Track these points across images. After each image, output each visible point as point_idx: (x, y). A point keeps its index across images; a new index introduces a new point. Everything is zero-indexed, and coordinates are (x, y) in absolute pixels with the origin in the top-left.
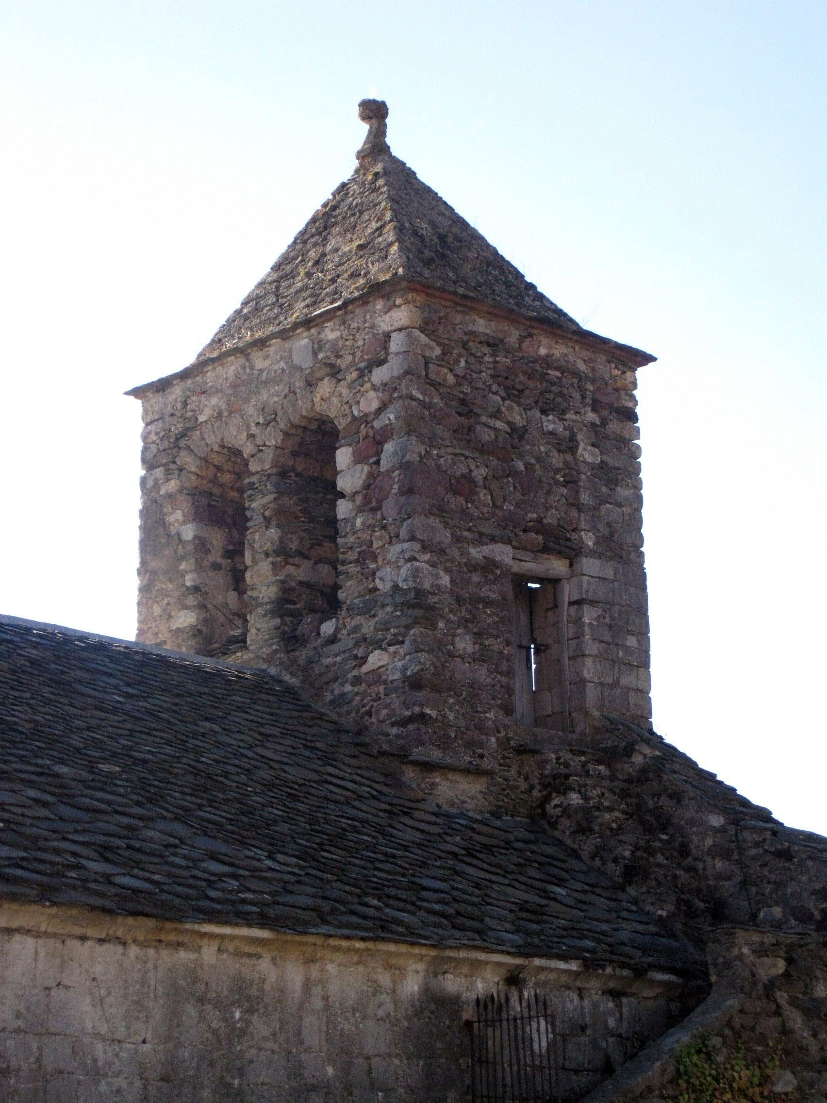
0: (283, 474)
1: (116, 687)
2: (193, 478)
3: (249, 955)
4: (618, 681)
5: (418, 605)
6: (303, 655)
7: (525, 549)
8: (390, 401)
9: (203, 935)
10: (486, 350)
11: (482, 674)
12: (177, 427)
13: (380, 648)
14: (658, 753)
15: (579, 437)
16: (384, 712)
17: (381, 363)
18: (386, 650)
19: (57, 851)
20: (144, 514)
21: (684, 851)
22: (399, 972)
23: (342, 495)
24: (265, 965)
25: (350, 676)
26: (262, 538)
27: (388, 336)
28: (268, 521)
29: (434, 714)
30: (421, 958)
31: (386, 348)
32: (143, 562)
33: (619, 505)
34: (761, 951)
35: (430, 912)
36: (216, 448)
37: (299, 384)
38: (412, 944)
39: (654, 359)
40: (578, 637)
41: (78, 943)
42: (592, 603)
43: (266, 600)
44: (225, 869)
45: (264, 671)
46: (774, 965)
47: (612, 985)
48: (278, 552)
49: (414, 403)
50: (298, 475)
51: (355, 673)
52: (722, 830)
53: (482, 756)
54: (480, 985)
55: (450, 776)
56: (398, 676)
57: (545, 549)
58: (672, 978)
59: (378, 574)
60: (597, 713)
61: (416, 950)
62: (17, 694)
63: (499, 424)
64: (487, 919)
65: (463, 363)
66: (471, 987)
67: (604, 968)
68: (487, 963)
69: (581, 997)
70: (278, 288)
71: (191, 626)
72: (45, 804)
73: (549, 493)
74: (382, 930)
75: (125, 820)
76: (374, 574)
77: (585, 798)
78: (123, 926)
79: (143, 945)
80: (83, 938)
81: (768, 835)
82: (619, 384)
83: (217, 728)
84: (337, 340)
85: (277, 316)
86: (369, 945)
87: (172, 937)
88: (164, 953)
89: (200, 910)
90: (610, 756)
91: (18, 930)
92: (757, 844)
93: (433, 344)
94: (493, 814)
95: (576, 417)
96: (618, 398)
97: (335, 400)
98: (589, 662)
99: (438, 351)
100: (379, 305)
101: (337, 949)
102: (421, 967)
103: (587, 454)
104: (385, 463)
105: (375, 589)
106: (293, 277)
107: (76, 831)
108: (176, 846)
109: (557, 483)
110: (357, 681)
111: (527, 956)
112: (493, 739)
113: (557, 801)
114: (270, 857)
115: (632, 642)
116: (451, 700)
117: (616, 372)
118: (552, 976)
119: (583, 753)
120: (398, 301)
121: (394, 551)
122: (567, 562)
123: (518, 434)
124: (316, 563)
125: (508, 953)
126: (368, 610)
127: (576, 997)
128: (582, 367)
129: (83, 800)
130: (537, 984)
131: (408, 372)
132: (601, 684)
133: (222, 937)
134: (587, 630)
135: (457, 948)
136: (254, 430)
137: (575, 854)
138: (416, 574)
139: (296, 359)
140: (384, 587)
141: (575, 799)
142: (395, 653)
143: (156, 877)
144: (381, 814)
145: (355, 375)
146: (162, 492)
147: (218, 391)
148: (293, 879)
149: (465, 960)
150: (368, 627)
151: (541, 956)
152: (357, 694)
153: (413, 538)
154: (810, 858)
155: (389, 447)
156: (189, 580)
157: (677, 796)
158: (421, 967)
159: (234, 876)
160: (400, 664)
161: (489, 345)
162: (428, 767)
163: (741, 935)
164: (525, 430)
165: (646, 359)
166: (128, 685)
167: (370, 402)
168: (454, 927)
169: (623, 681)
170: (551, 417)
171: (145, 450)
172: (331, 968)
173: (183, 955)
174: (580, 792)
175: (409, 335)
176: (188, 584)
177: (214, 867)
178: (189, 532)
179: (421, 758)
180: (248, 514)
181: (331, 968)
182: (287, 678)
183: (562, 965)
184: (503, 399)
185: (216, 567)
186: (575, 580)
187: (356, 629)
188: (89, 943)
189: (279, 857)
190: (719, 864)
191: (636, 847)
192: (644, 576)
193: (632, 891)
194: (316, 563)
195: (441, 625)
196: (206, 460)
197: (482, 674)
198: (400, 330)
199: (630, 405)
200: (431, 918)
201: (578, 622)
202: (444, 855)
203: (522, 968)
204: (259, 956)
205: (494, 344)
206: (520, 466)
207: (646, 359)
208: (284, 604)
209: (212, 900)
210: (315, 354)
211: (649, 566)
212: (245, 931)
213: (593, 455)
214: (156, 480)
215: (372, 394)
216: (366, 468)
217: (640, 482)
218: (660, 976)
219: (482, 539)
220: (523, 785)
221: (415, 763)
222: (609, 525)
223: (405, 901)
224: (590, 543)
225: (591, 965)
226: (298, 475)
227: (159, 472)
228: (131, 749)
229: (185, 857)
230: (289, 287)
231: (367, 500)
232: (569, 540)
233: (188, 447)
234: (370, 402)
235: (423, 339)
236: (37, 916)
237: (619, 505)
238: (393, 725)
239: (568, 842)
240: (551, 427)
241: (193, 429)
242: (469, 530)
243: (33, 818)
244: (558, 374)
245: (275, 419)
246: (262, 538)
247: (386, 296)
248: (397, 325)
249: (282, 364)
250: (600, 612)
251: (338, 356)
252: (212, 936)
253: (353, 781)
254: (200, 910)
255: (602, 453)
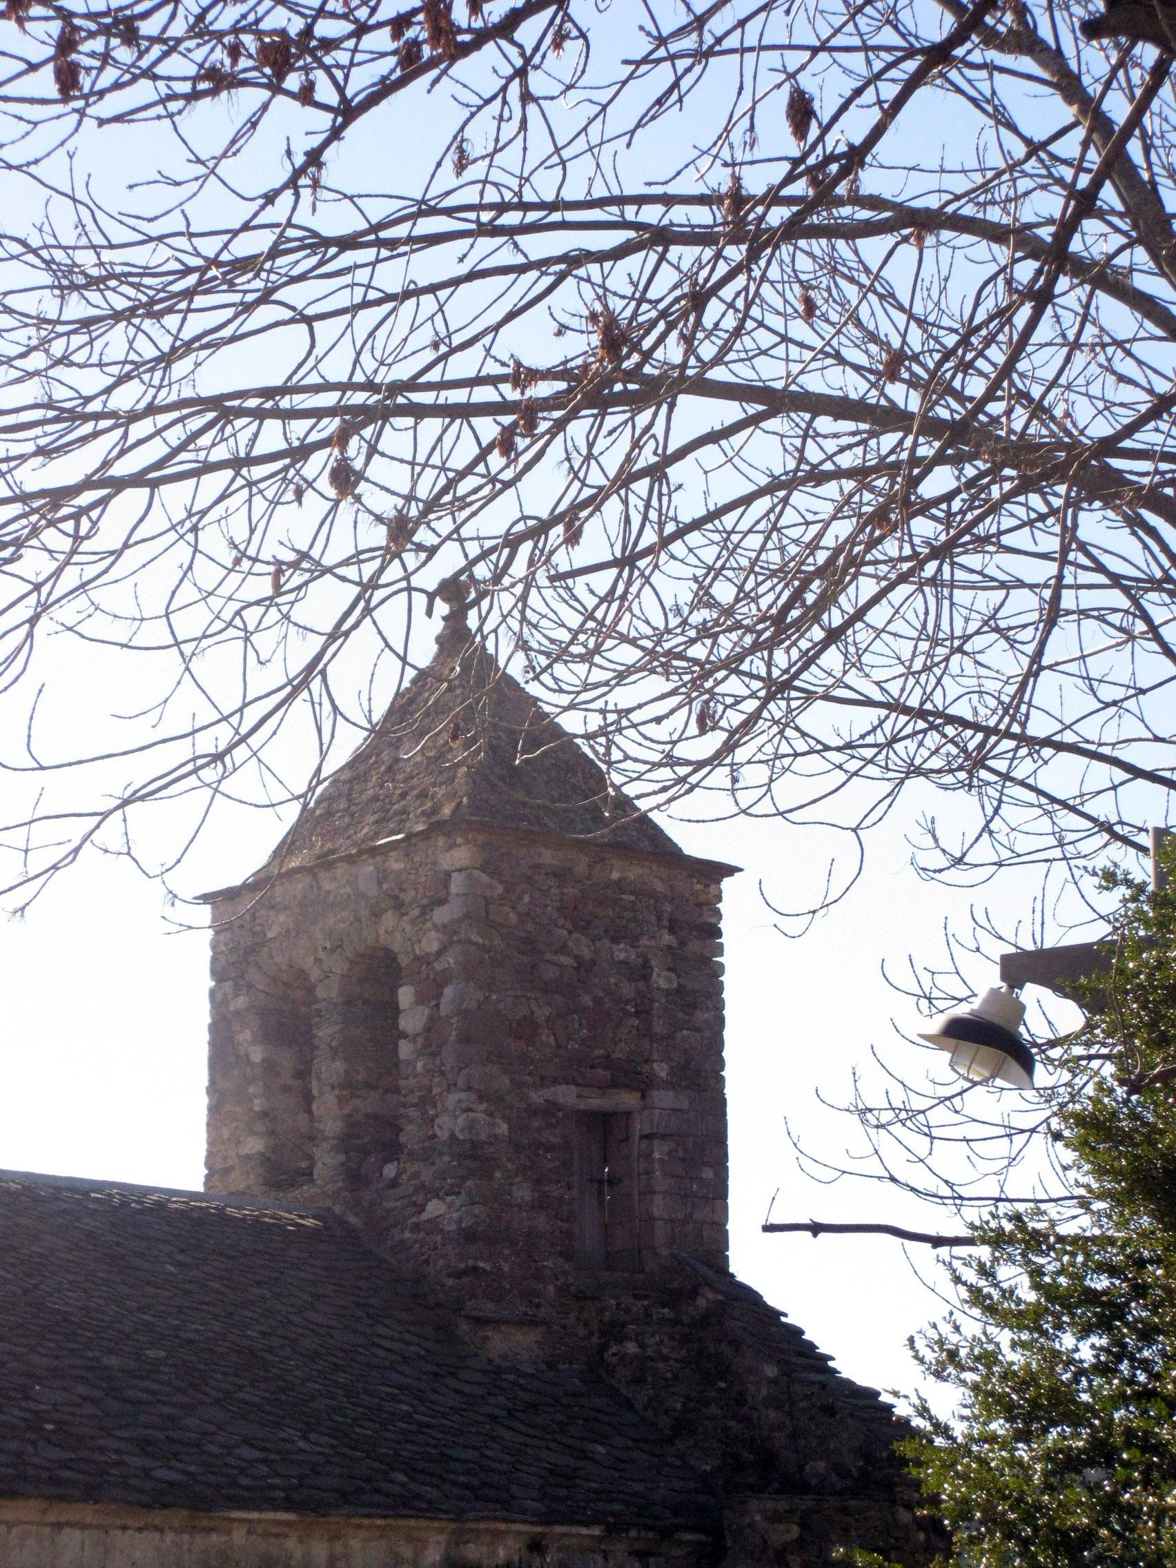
0: (350, 1002)
1: (169, 1255)
2: (262, 996)
3: (277, 1536)
4: (691, 1215)
5: (475, 1156)
6: (366, 1195)
7: (590, 1086)
8: (451, 944)
9: (234, 1520)
10: (552, 882)
11: (541, 1222)
12: (247, 941)
13: (437, 1196)
14: (720, 1297)
15: (653, 963)
16: (441, 1262)
17: (442, 902)
18: (443, 1199)
19: (102, 1450)
20: (214, 1028)
21: (741, 1399)
22: (422, 1544)
23: (404, 1035)
24: (291, 1544)
25: (410, 1222)
26: (329, 1069)
27: (448, 875)
28: (334, 1053)
29: (488, 1267)
30: (441, 1531)
31: (447, 887)
32: (212, 1081)
33: (698, 1030)
34: (775, 1518)
35: (454, 1483)
36: (284, 968)
37: (364, 913)
38: (432, 1519)
39: (741, 870)
40: (648, 1173)
41: (119, 1533)
42: (663, 1137)
43: (332, 1134)
44: (258, 1454)
45: (329, 1209)
46: (788, 1531)
47: (637, 1546)
48: (343, 1086)
49: (473, 948)
50: (366, 1002)
51: (414, 1220)
52: (774, 1382)
53: (538, 1306)
54: (502, 1552)
55: (503, 1328)
56: (453, 1227)
57: (614, 1085)
58: (702, 1537)
59: (437, 1121)
60: (665, 1252)
61: (437, 1524)
62: (70, 1277)
63: (565, 960)
64: (514, 1487)
65: (527, 899)
66: (494, 1553)
67: (627, 1531)
68: (508, 1532)
69: (605, 1558)
70: (351, 790)
71: (260, 1153)
72: (93, 1401)
73: (617, 1027)
74: (405, 1505)
75: (167, 1410)
76: (433, 1121)
77: (642, 1346)
78: (157, 1517)
79: (178, 1531)
80: (124, 1528)
81: (816, 1388)
82: (702, 898)
83: (268, 1294)
84: (400, 871)
85: (348, 827)
86: (390, 1521)
87: (205, 1523)
88: (198, 1537)
89: (230, 1498)
90: (674, 1298)
91: (68, 1524)
92: (807, 1397)
93: (495, 883)
94: (548, 1364)
95: (652, 943)
96: (701, 915)
97: (398, 935)
98: (658, 1199)
99: (500, 890)
100: (441, 841)
101: (359, 1527)
102: (442, 1538)
103: (662, 980)
104: (444, 1010)
105: (434, 1136)
106: (366, 781)
107: (120, 1427)
108: (214, 1434)
109: (627, 1013)
110: (416, 1228)
111: (548, 1524)
112: (551, 1288)
113: (614, 1349)
114: (304, 1437)
115: (708, 1173)
116: (506, 1252)
117: (699, 887)
118: (574, 1541)
119: (646, 1297)
120: (459, 840)
121: (453, 1098)
122: (639, 1095)
123: (585, 967)
124: (386, 1092)
125: (531, 1523)
126: (427, 1156)
127: (600, 1560)
128: (659, 886)
129: (130, 1392)
130: (559, 1549)
131: (467, 916)
132: (672, 1221)
133: (251, 1521)
134: (657, 1166)
135: (477, 1520)
136: (321, 955)
137: (630, 1405)
138: (471, 1125)
139: (362, 886)
140: (443, 1135)
141: (631, 1348)
142: (453, 1202)
143: (192, 1468)
144: (425, 1377)
145: (417, 912)
146: (232, 1008)
147: (287, 908)
148: (322, 1459)
149: (487, 1530)
150: (427, 1175)
151: (562, 1523)
152: (416, 1241)
153: (469, 1089)
154: (851, 1415)
155: (448, 992)
156: (258, 1105)
157: (735, 1344)
158: (442, 1538)
159: (265, 1461)
160: (455, 1215)
161: (555, 875)
162: (480, 1322)
163: (753, 1505)
164: (594, 962)
165: (731, 870)
166: (182, 1251)
167: (431, 943)
168: (477, 1498)
169: (697, 1215)
170: (622, 946)
171: (214, 960)
172: (355, 1544)
173: (214, 1538)
174: (637, 1341)
175: (469, 877)
176: (257, 1109)
177: (246, 1452)
178: (257, 1054)
179: (474, 1313)
180: (315, 1041)
181: (355, 1544)
182: (352, 1219)
183: (584, 1531)
184: (570, 933)
185: (286, 1089)
186: (645, 1113)
187: (415, 1175)
188: (130, 1532)
189: (312, 1436)
190: (772, 1414)
191: (689, 1399)
192: (723, 1102)
193: (680, 1445)
194: (386, 1092)
195: (498, 1175)
196: (274, 979)
197: (541, 1222)
198: (460, 870)
199: (713, 920)
200: (455, 1491)
201: (649, 1156)
202: (481, 1418)
203: (543, 1535)
204: (286, 1536)
205: (562, 875)
206: (587, 1000)
207: (731, 870)
208: (346, 1142)
209: (242, 1487)
210: (380, 884)
211: (730, 1091)
212: (271, 1515)
213: (669, 980)
214: (226, 994)
215: (433, 934)
216: (427, 1011)
217: (722, 1002)
218: (687, 1537)
219: (543, 1082)
220: (582, 1332)
221: (468, 1317)
222: (685, 1052)
223: (432, 1474)
224: (663, 1075)
225: (614, 1529)
226: (366, 1002)
227: (228, 986)
228: (178, 1328)
229: (221, 1445)
230: (362, 792)
231: (427, 1044)
232: (639, 1073)
233: (257, 964)
234: (431, 943)
235: (484, 878)
236: (86, 1512)
237: (698, 1030)
238: (450, 1275)
239: (624, 1391)
240: (622, 956)
241: (262, 945)
242: (530, 1074)
243: (81, 1416)
244: (632, 898)
245: (341, 946)
246: (329, 1069)
247: (448, 834)
248: (458, 866)
249: (348, 889)
250: (672, 1145)
251: (401, 890)
252: (242, 1521)
253: (401, 1341)
254: (230, 1498)
255: (679, 976)
